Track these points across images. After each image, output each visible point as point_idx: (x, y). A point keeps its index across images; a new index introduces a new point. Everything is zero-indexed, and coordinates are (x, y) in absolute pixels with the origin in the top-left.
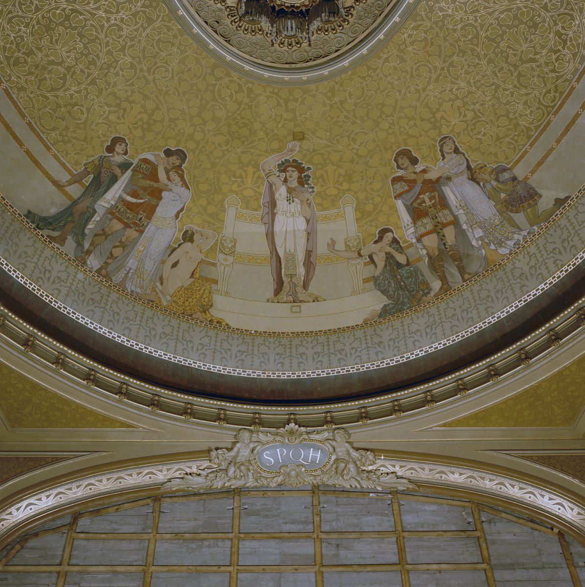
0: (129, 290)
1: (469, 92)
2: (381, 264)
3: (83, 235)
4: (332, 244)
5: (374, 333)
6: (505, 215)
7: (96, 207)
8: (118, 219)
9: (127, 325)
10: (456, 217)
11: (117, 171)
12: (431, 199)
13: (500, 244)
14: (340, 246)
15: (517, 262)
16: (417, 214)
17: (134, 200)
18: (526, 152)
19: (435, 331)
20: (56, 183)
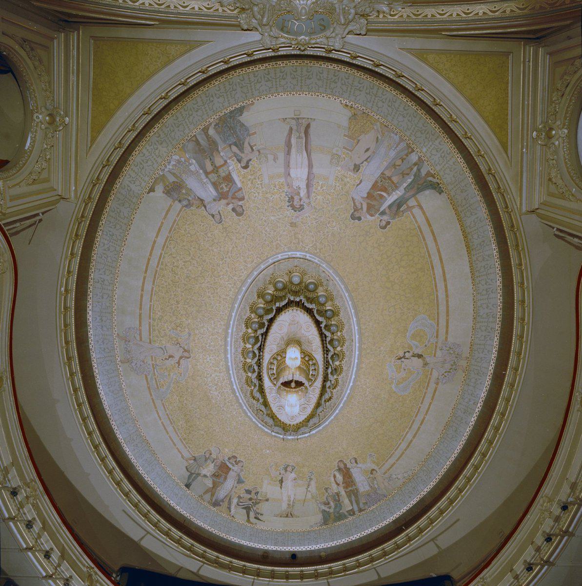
0: (398, 136)
1: (211, 246)
2: (246, 145)
3: (415, 176)
4: (275, 159)
5: (247, 95)
6: (181, 180)
7: (403, 192)
8: (393, 183)
9: (405, 112)
10: (207, 177)
11: (387, 211)
12: (222, 188)
13: (179, 162)
14: (271, 157)
15: (166, 151)
16: (229, 179)
17: (383, 193)
18: (177, 216)
19: (207, 98)
20: (421, 208)
